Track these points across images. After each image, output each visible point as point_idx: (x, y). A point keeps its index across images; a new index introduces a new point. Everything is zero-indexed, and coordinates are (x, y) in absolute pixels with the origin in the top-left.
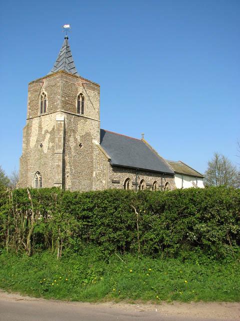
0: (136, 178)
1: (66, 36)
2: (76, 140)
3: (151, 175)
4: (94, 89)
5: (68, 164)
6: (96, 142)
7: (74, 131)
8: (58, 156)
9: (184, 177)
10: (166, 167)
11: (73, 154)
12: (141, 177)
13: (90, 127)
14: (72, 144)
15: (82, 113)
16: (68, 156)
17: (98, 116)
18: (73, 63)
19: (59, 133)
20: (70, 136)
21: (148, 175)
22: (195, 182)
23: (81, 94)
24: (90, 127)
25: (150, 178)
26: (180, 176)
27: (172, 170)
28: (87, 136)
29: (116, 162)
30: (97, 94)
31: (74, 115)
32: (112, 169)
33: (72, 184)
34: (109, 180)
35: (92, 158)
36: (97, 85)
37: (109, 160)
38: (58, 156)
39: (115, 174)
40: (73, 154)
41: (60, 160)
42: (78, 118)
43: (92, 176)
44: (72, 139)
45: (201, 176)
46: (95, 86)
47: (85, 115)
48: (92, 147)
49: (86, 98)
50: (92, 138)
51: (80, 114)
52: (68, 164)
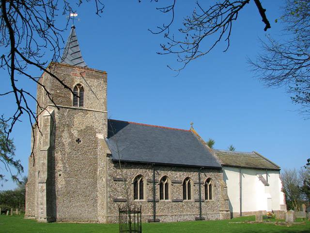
0: (154, 174)
1: (73, 25)
2: (71, 135)
3: (180, 171)
4: (98, 78)
5: (60, 162)
6: (101, 136)
7: (69, 126)
8: (43, 154)
9: (243, 170)
10: (213, 159)
11: (68, 150)
12: (162, 173)
13: (94, 115)
14: (65, 138)
15: (81, 105)
16: (60, 153)
17: (104, 107)
18: (78, 47)
19: (46, 129)
20: (63, 131)
21: (175, 171)
22: (264, 176)
23: (79, 85)
24: (94, 115)
25: (178, 174)
26: (237, 169)
27: (220, 162)
28: (89, 131)
29: (116, 157)
30: (102, 82)
31: (68, 108)
32: (113, 165)
33: (67, 183)
34: (109, 178)
35: (96, 154)
36: (102, 73)
37: (108, 155)
38: (43, 154)
39: (119, 171)
40: (68, 150)
41: (44, 157)
42: (74, 111)
43: (95, 173)
44: (65, 134)
45: (274, 168)
46: (101, 74)
47: (85, 107)
48: (96, 141)
49: (86, 89)
50: (96, 133)
51: (78, 107)
52: (60, 162)
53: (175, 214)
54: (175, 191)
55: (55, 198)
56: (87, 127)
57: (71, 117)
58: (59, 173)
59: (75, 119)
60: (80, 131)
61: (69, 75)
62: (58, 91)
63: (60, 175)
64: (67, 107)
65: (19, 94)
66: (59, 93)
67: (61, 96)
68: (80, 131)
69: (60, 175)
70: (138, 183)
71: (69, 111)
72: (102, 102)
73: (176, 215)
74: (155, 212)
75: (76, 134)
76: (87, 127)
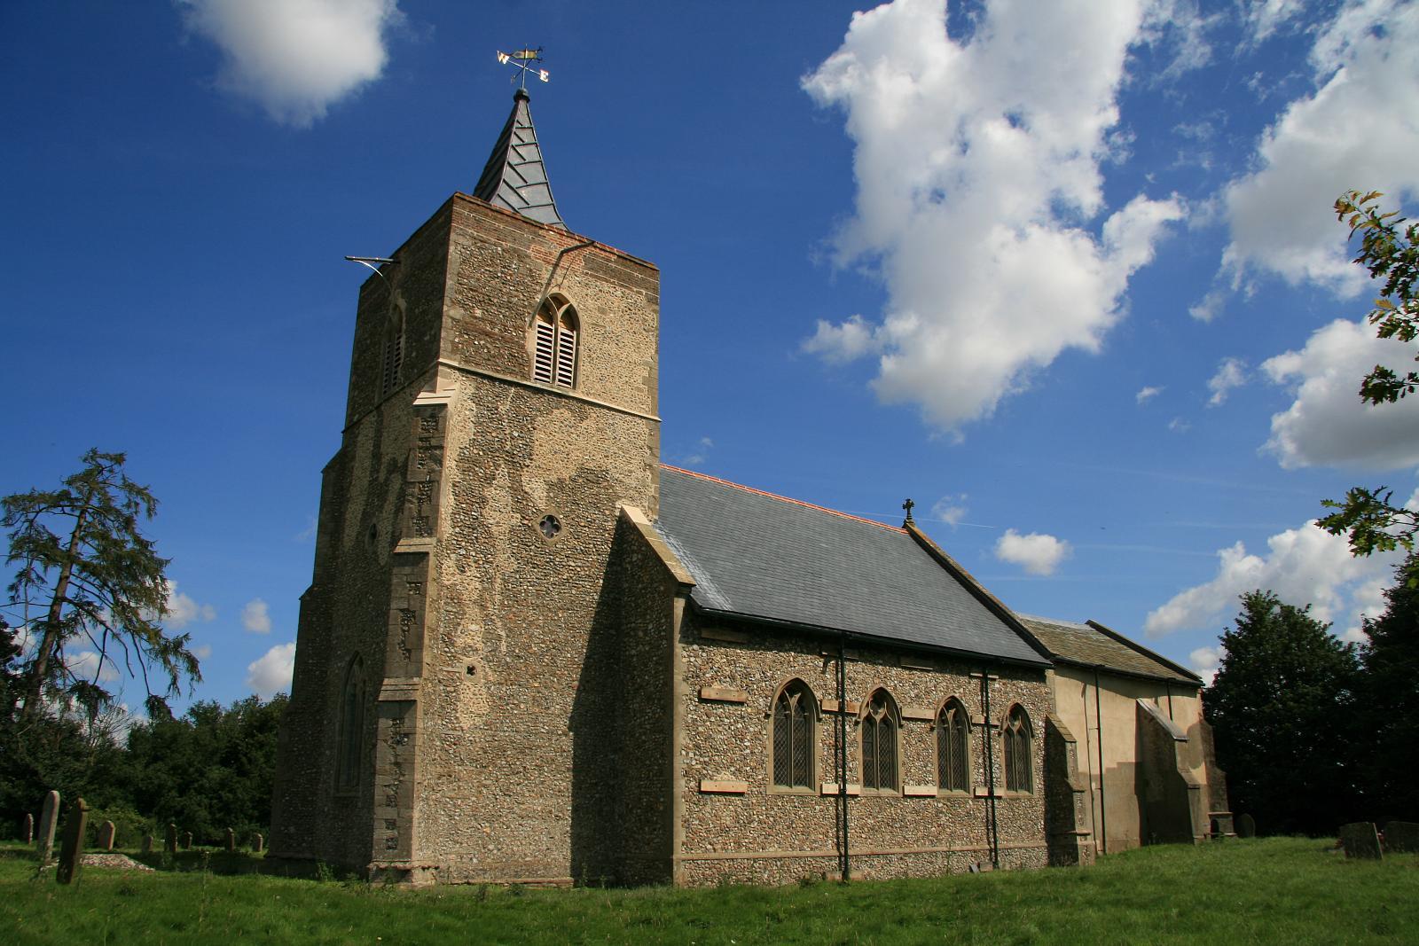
2: (520, 496)
42: (535, 400)
53: (915, 848)
54: (916, 752)
55: (748, 645)
56: (582, 470)
57: (524, 423)
58: (467, 661)
59: (537, 435)
60: (556, 486)
61: (522, 257)
62: (478, 313)
63: (471, 670)
64: (509, 378)
65: (152, 503)
66: (482, 319)
67: (487, 334)
68: (556, 486)
69: (471, 670)
70: (796, 705)
71: (517, 394)
72: (640, 381)
73: (916, 854)
74: (842, 843)
75: (537, 491)
76: (582, 470)
